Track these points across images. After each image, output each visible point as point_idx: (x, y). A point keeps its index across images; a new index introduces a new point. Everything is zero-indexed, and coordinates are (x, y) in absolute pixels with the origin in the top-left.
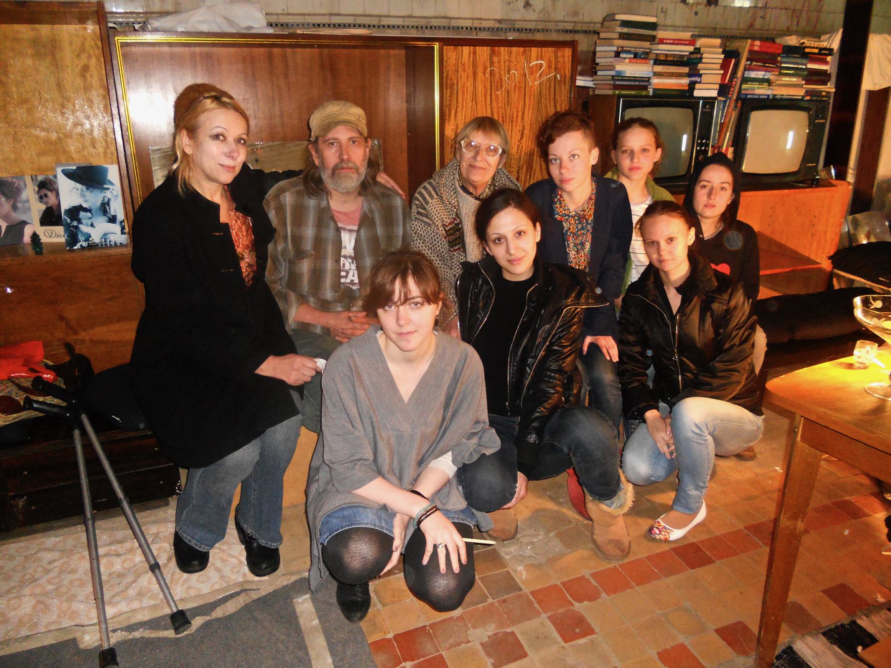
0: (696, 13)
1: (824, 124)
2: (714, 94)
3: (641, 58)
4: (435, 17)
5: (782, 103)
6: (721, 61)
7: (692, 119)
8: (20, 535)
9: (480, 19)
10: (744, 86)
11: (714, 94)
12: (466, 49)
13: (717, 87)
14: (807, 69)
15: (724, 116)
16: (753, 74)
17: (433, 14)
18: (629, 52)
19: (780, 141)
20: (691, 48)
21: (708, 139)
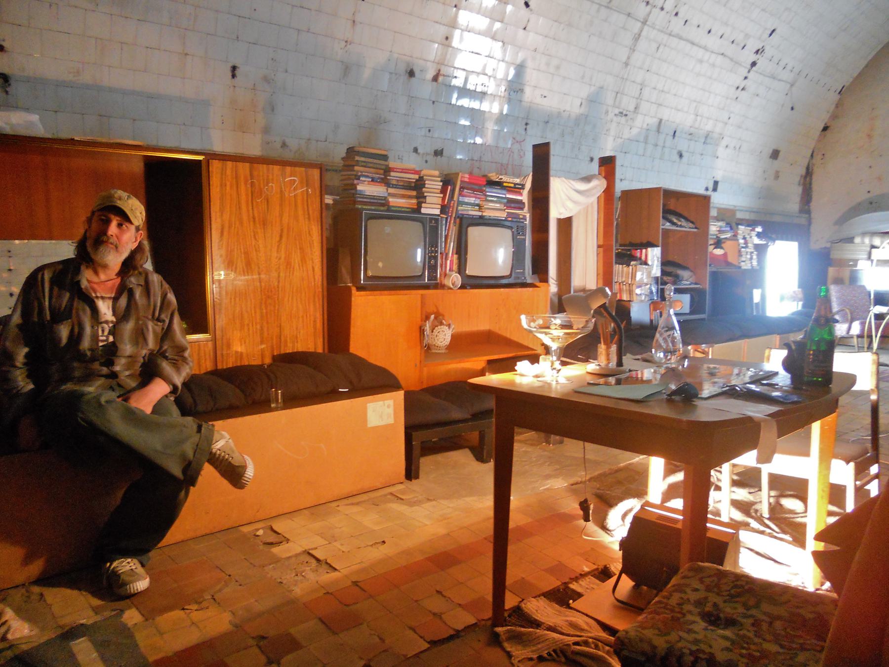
0: (426, 162)
1: (525, 240)
2: (437, 212)
5: (490, 222)
6: (440, 187)
7: (422, 235)
10: (460, 208)
11: (437, 212)
12: (229, 164)
13: (439, 207)
14: (506, 198)
15: (448, 232)
16: (466, 200)
18: (367, 177)
19: (495, 254)
20: (417, 177)
21: (437, 247)
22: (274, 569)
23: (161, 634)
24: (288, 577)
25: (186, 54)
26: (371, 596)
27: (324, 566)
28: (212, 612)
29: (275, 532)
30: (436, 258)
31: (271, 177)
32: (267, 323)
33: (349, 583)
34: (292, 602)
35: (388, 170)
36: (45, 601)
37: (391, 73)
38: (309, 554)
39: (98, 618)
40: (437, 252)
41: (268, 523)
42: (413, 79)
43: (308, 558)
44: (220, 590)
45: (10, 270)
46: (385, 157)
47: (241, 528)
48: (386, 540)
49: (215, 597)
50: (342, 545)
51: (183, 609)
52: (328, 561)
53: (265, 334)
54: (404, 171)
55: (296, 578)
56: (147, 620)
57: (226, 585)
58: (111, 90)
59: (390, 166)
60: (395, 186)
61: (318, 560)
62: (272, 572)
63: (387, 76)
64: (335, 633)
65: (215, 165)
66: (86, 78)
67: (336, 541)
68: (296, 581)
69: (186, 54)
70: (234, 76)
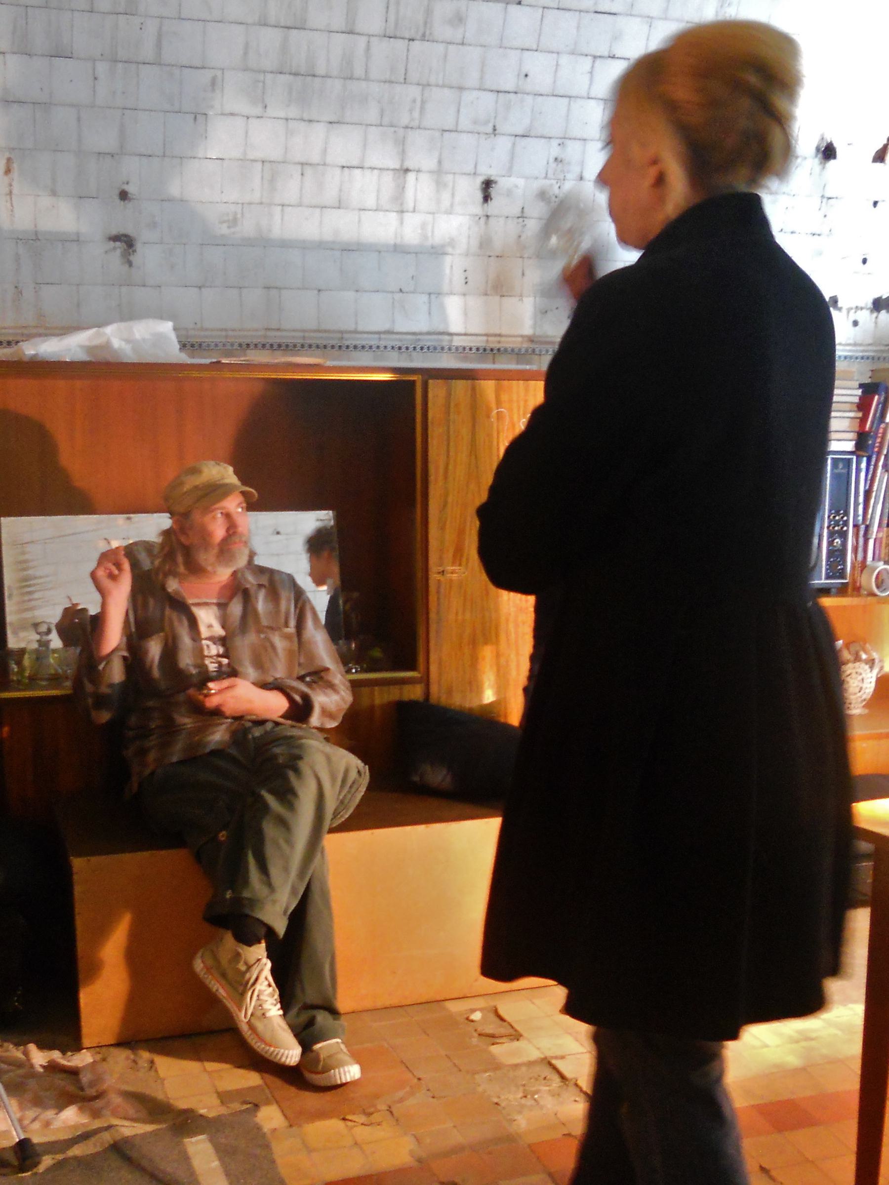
0: (855, 323)
4: (429, 333)
8: (331, 927)
9: (500, 335)
17: (425, 329)
21: (846, 513)
22: (490, 1079)
23: (310, 1150)
24: (511, 1097)
25: (407, 170)
27: (572, 1089)
29: (502, 1019)
30: (843, 535)
34: (511, 1139)
36: (156, 1071)
38: (550, 1064)
39: (223, 1111)
40: (846, 523)
41: (492, 1003)
44: (401, 1100)
49: (394, 1110)
51: (344, 1119)
55: (523, 1101)
56: (291, 1126)
57: (412, 1094)
58: (285, 244)
61: (563, 1077)
62: (485, 1083)
65: (437, 390)
66: (247, 228)
68: (522, 1106)
69: (407, 170)
70: (487, 198)
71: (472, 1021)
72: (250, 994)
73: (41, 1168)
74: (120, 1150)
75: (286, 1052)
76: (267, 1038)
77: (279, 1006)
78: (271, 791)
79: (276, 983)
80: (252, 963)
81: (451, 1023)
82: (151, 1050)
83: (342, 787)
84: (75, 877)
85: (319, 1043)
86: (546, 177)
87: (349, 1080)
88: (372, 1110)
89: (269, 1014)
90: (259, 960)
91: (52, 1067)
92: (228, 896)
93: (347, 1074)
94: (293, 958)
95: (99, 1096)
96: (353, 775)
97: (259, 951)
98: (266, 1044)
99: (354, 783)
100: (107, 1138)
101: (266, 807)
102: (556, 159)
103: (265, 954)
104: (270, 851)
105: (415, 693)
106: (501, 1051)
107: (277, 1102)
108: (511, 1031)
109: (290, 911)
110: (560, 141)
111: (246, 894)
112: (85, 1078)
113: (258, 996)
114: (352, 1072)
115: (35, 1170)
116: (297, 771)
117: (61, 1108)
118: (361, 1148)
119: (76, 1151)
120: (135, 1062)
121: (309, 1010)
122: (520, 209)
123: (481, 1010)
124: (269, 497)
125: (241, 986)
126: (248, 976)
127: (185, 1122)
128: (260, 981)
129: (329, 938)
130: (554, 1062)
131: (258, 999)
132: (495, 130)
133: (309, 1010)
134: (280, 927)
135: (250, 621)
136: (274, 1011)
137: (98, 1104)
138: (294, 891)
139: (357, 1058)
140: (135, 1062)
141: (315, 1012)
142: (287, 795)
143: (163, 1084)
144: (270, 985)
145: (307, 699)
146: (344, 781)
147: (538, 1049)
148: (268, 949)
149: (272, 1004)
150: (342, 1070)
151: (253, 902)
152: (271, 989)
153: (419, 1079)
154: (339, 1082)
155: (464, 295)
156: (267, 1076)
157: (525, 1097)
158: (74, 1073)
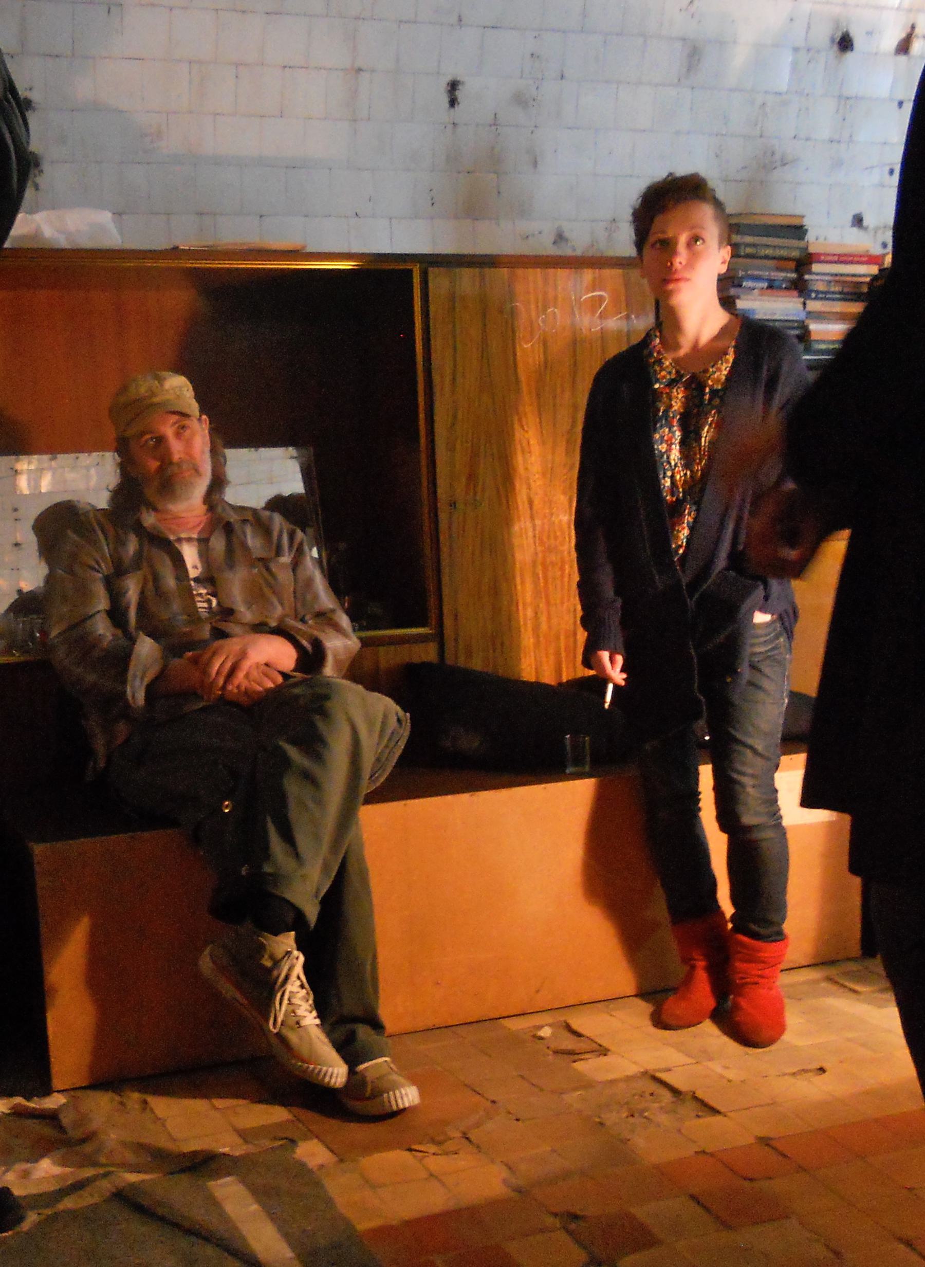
3: (780, 288)
25: (360, 70)
26: (801, 1169)
28: (464, 1161)
31: (551, 294)
32: (548, 603)
33: (752, 1140)
35: (804, 262)
37: (796, 50)
42: (849, 56)
43: (654, 1087)
44: (478, 1125)
45: (17, 545)
46: (798, 231)
47: (506, 1022)
48: (825, 1065)
49: (469, 1135)
50: (727, 1068)
51: (410, 1150)
52: (700, 1094)
53: (544, 627)
54: (844, 259)
55: (631, 1120)
59: (812, 250)
60: (824, 296)
61: (675, 1091)
63: (787, 58)
64: (726, 1225)
65: (439, 282)
67: (711, 1059)
70: (453, 102)
71: (541, 1038)
72: (279, 995)
73: (26, 1226)
74: (125, 1198)
75: (330, 1070)
76: (305, 1052)
77: (314, 1013)
78: (294, 742)
79: (309, 984)
80: (280, 956)
81: (515, 1040)
82: (144, 1090)
83: (381, 736)
84: (37, 868)
85: (362, 1063)
86: (521, 77)
87: (407, 1105)
88: (441, 1138)
89: (304, 1023)
90: (288, 953)
91: (18, 1113)
92: (244, 873)
93: (405, 1099)
94: (334, 949)
95: (88, 1138)
96: (393, 721)
97: (287, 941)
98: (303, 1061)
99: (393, 733)
100: (106, 1186)
101: (286, 762)
102: (532, 55)
103: (295, 946)
104: (294, 812)
105: (428, 653)
106: (587, 1066)
107: (317, 1137)
108: (594, 1045)
109: (322, 894)
110: (536, 34)
111: (267, 869)
112: (66, 1119)
113: (289, 1000)
114: (408, 1096)
115: (18, 1229)
116: (325, 714)
117: (35, 1158)
118: (440, 1180)
119: (68, 1203)
120: (122, 1103)
121: (350, 1019)
122: (493, 116)
123: (550, 1025)
124: (238, 426)
125: (266, 987)
126: (275, 973)
127: (202, 1164)
128: (290, 981)
129: (370, 931)
130: (658, 1075)
131: (290, 1004)
132: (460, 20)
133: (350, 1019)
134: (312, 912)
135: (239, 553)
136: (310, 1019)
137: (88, 1148)
138: (326, 867)
139: (414, 1080)
140: (122, 1103)
141: (356, 1026)
142: (314, 744)
143: (164, 1125)
144: (302, 986)
145: (318, 645)
146: (382, 731)
147: (635, 1063)
148: (297, 941)
149: (306, 1010)
150: (397, 1092)
151: (276, 878)
152: (304, 991)
153: (493, 1102)
154: (395, 1108)
155: (432, 218)
156: (296, 1110)
157: (632, 1116)
158: (51, 1117)
